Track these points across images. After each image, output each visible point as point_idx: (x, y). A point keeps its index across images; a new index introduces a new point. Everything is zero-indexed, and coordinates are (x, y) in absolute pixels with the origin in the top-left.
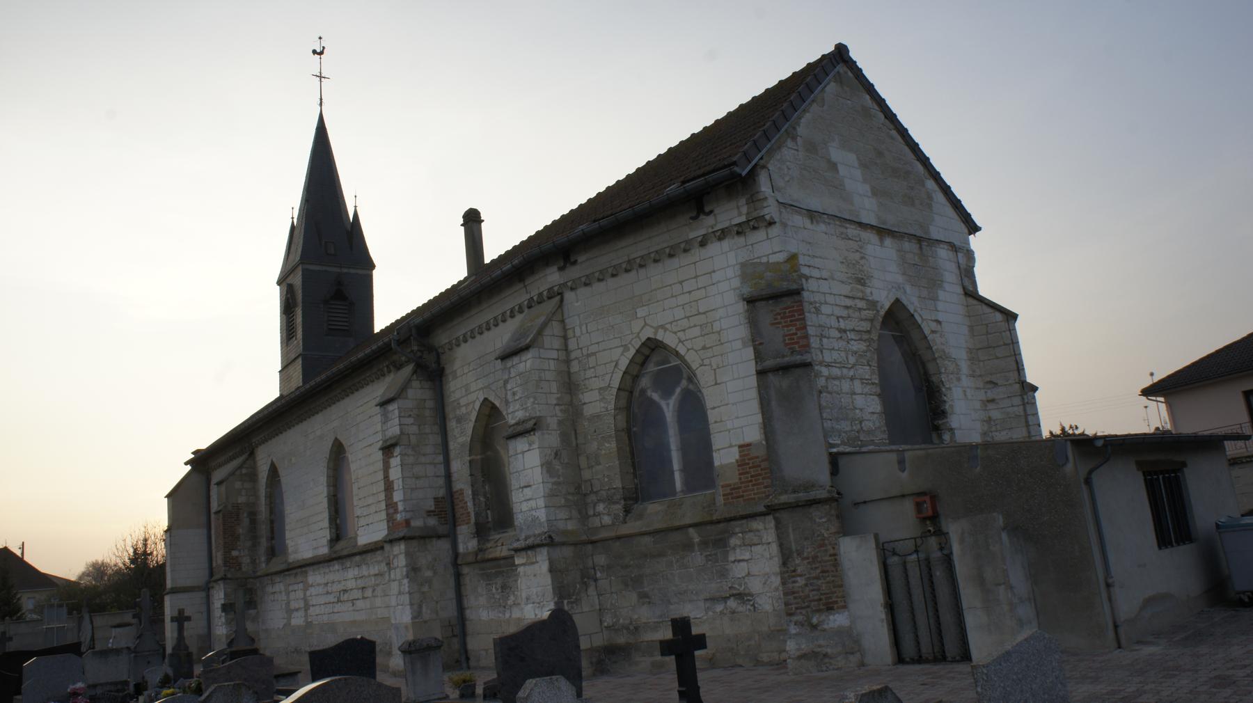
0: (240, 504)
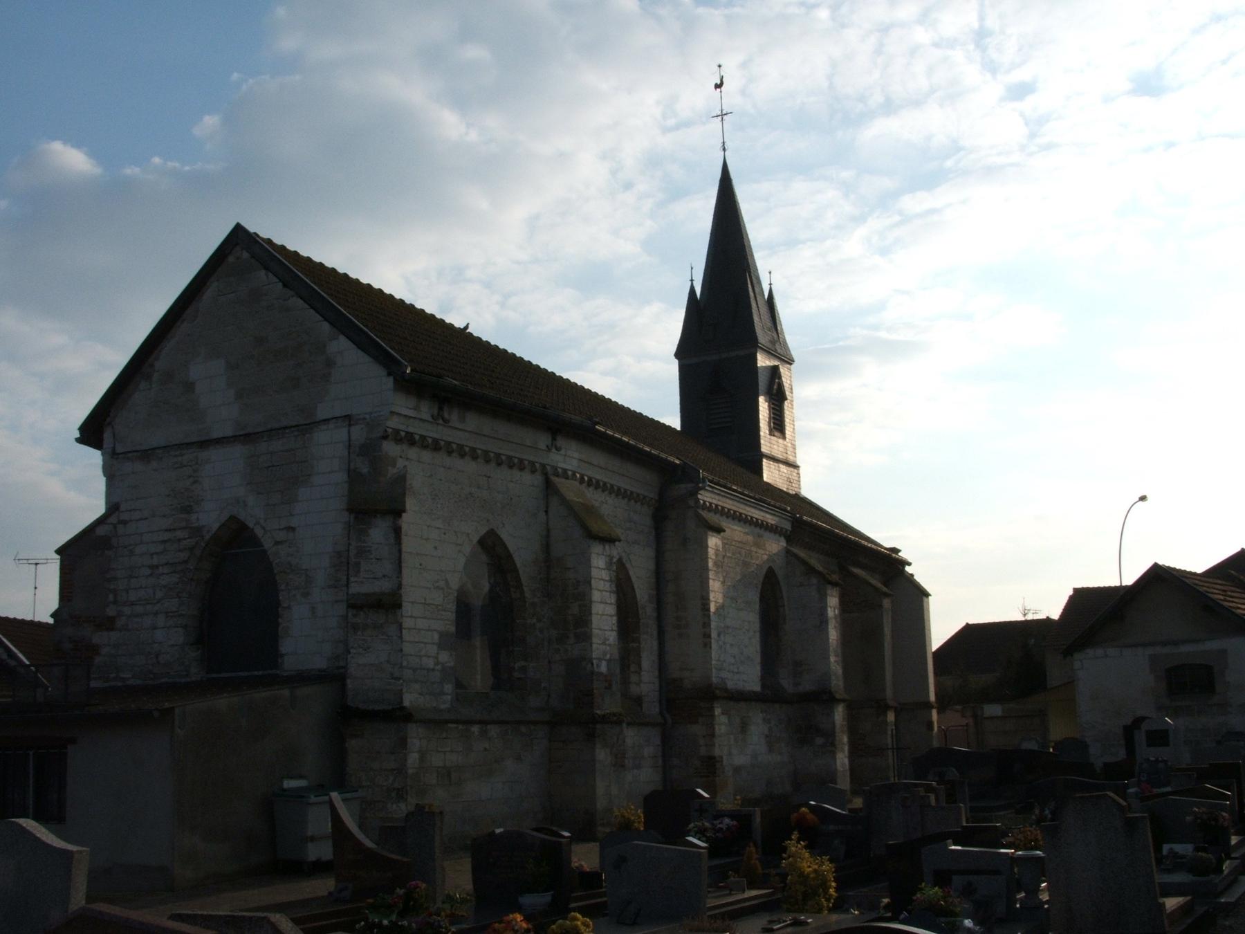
0: (611, 577)
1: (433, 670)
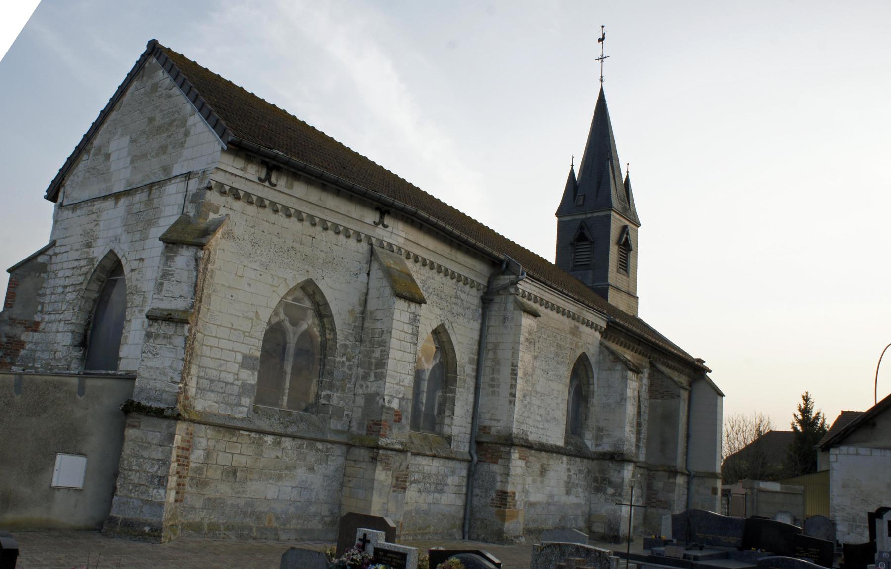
1: (232, 384)
